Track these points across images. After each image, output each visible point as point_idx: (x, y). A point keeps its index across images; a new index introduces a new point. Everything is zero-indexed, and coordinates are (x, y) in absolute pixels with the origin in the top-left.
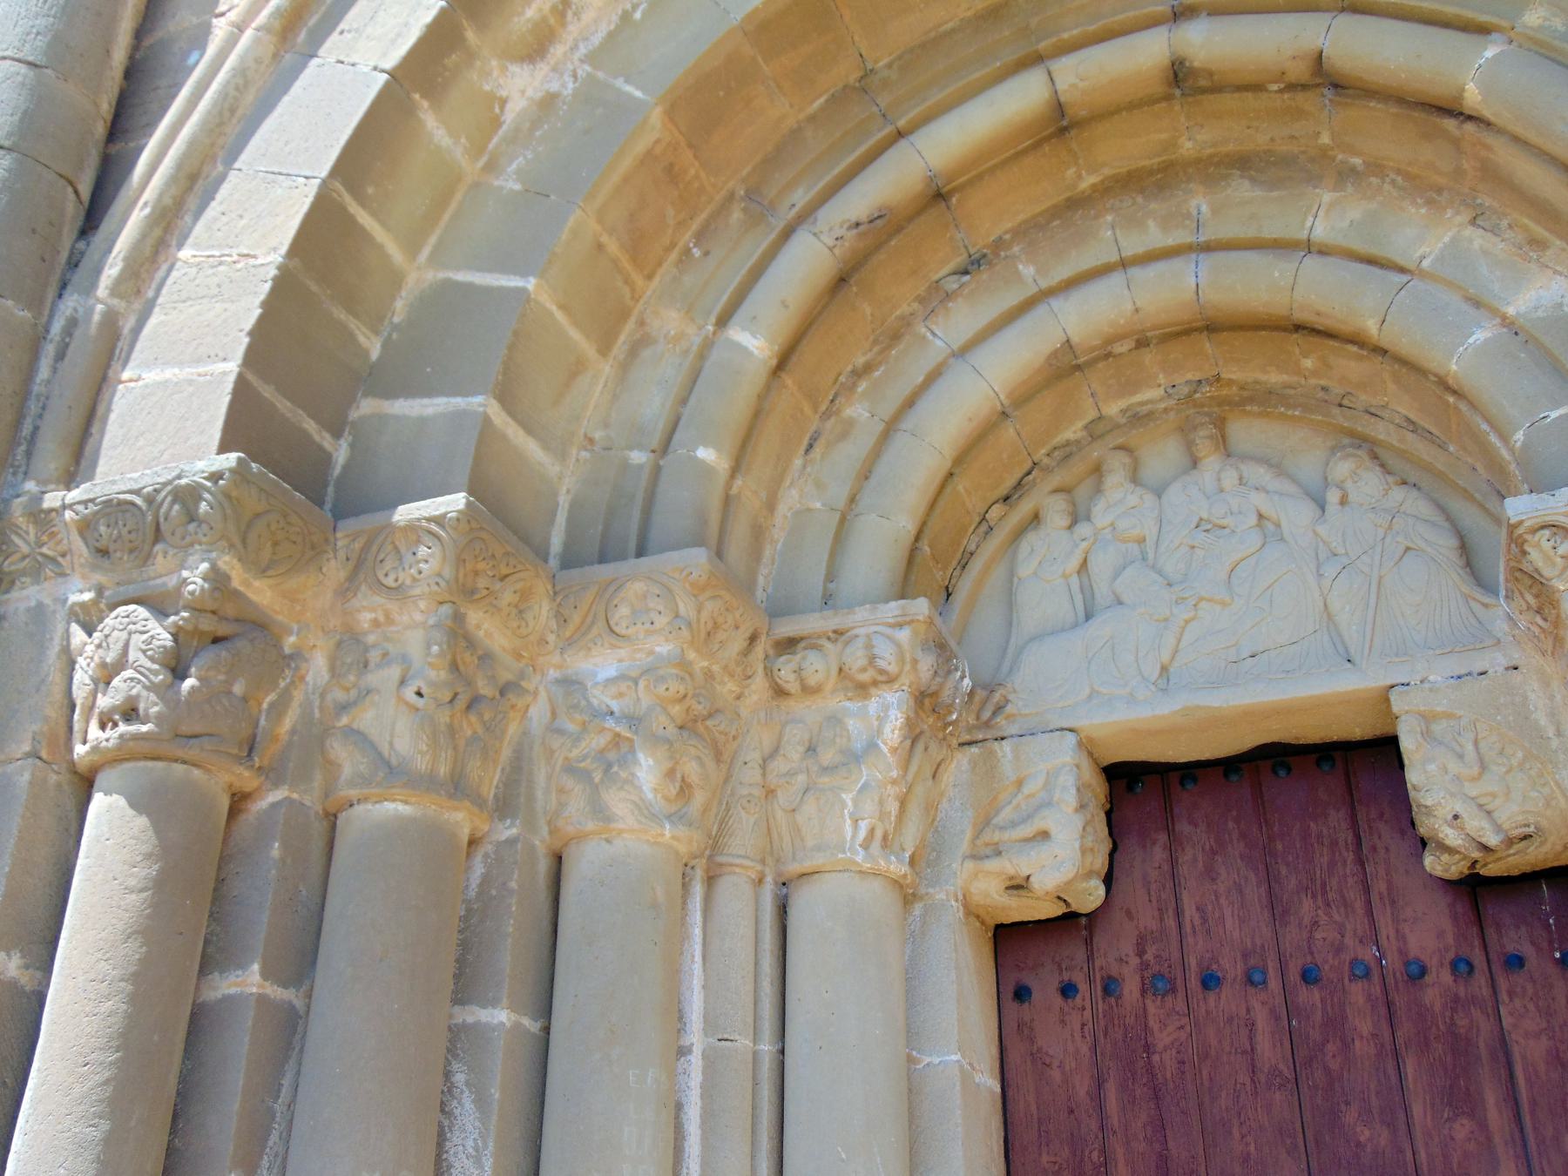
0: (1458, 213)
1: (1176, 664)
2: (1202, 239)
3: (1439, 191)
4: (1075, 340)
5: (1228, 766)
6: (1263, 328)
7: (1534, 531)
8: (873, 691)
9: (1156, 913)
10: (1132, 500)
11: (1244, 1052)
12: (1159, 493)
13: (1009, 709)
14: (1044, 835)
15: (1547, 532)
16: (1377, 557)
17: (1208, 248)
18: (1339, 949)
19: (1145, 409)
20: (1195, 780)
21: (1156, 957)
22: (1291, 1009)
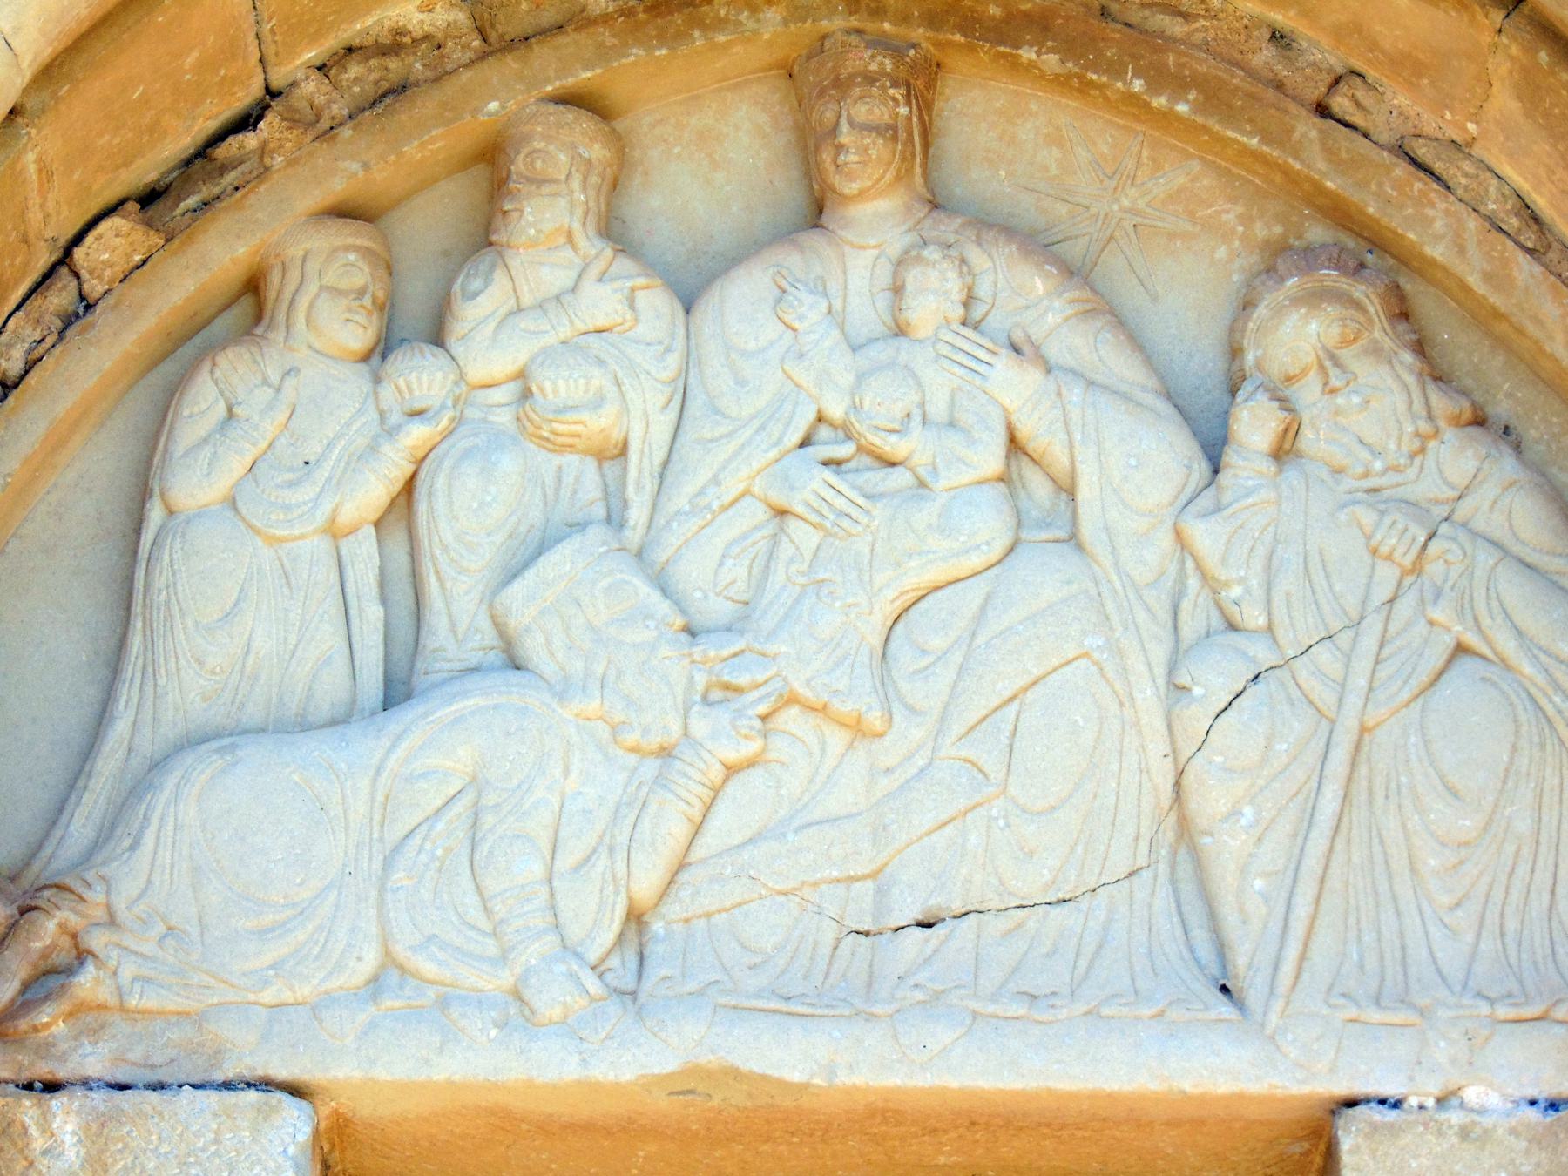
1: (673, 910)
10: (601, 302)
13: (87, 982)
16: (1362, 666)
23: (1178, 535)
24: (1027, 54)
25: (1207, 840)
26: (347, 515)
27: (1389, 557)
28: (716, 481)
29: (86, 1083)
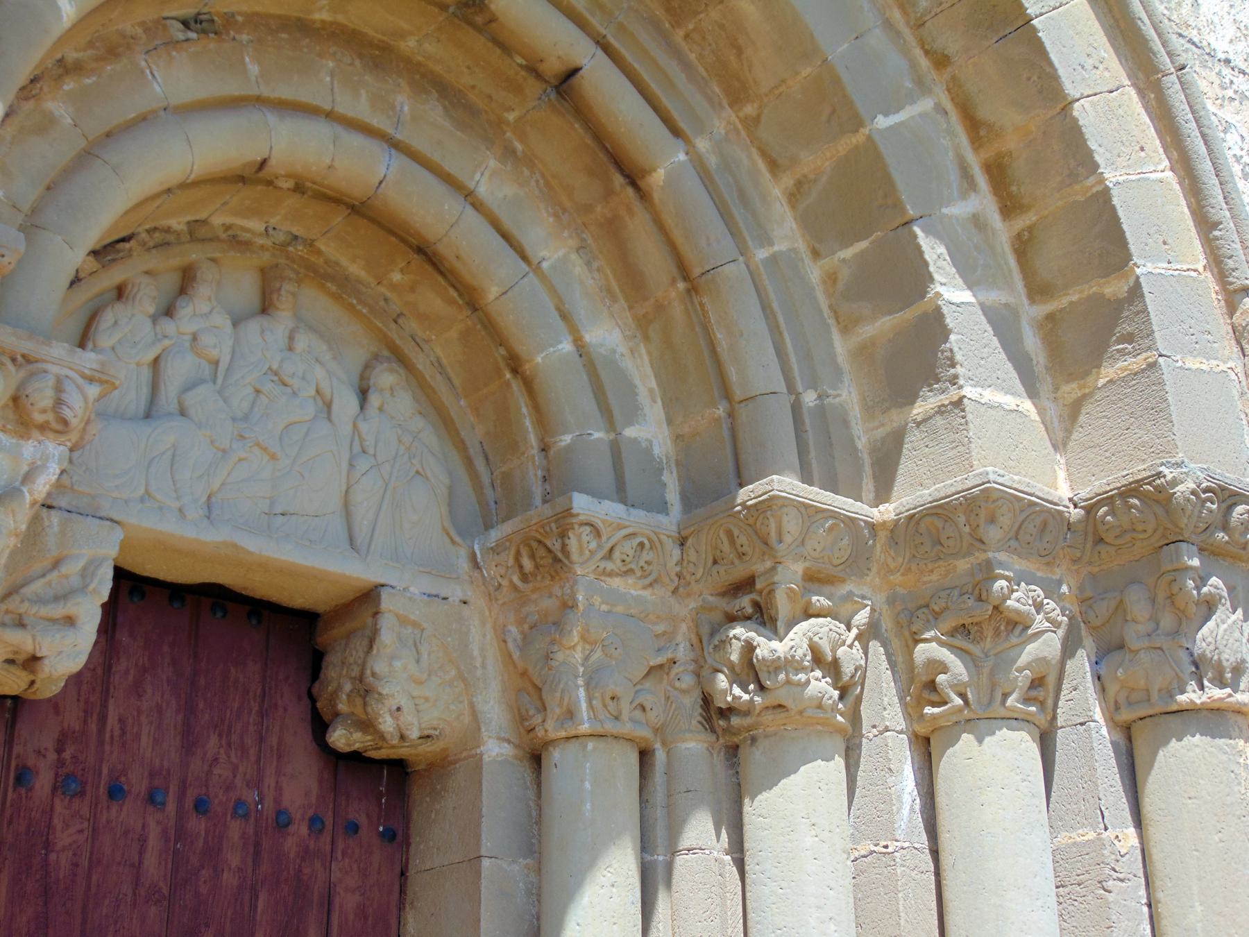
0: (571, 237)
2: (398, 136)
4: (273, 161)
5: (177, 592)
6: (395, 235)
8: (36, 434)
9: (81, 714)
11: (132, 865)
14: (70, 621)
15: (588, 529)
17: (396, 145)
18: (229, 787)
19: (247, 236)
20: (143, 596)
21: (74, 757)
22: (181, 833)
23: (355, 426)
24: (329, 285)
28: (243, 377)
29: (60, 509)
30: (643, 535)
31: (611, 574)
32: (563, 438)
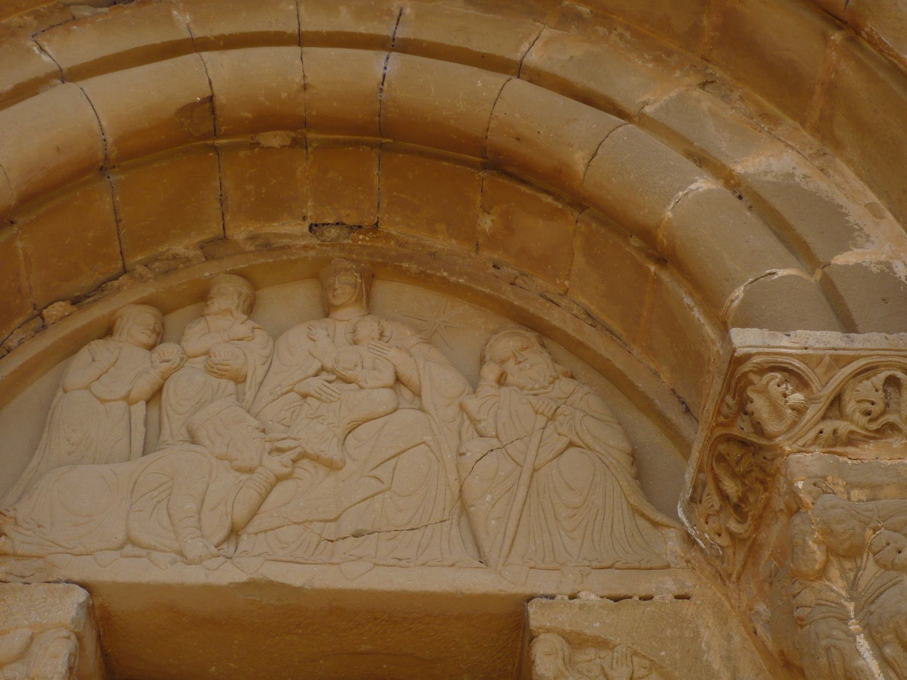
3: (670, 53)
4: (221, 99)
7: (762, 370)
12: (276, 335)
15: (779, 375)
19: (286, 241)
25: (473, 508)
26: (134, 394)
27: (542, 414)
30: (888, 366)
31: (851, 440)
32: (733, 296)
